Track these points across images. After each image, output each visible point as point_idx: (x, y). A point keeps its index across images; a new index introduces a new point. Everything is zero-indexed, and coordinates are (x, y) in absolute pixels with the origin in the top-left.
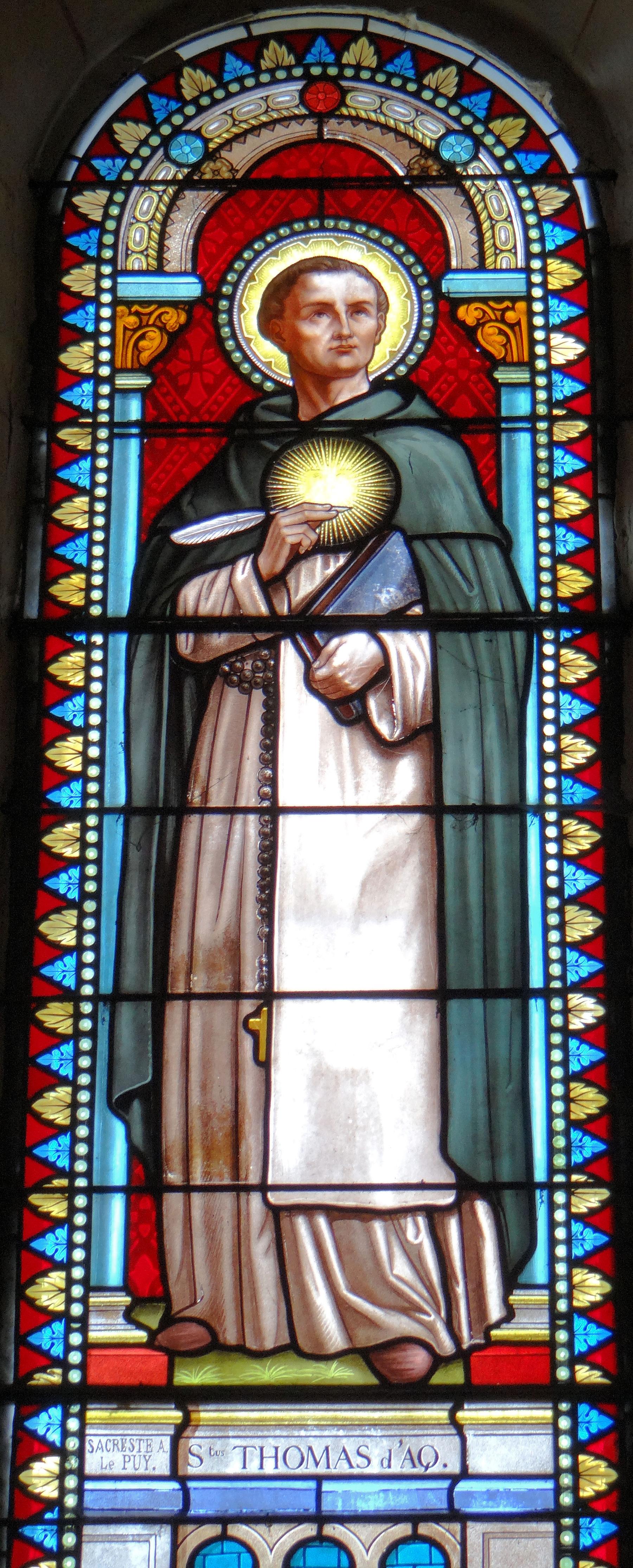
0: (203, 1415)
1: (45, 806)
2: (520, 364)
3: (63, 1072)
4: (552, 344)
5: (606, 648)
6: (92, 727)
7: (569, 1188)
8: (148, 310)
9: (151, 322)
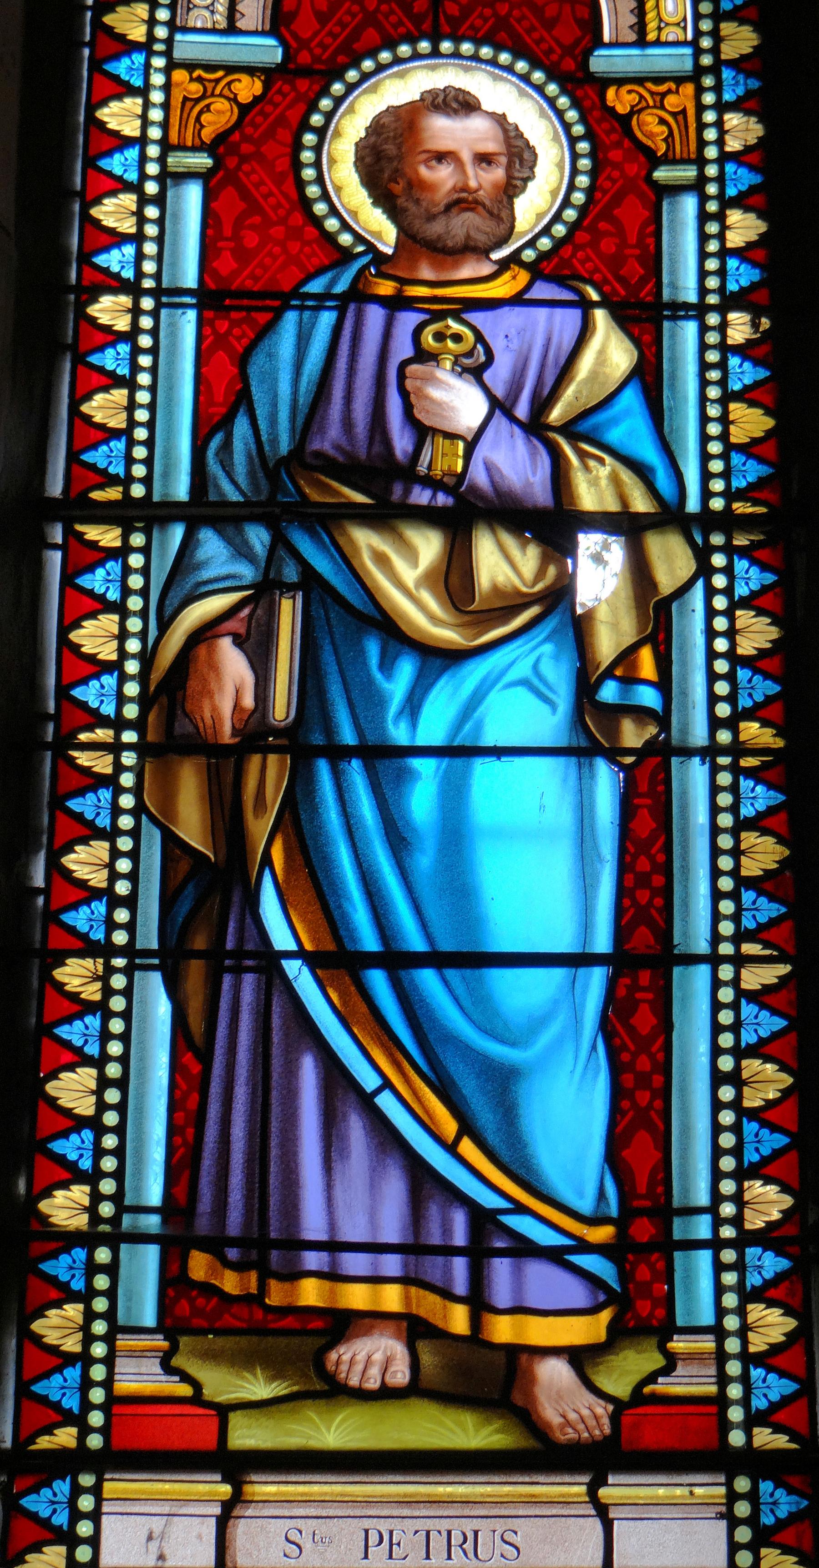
0: (258, 1488)
1: (35, 1226)
2: (685, 161)
3: (112, 424)
4: (728, 223)
5: (811, 1221)
6: (111, 1059)
7: (739, 961)
8: (212, 76)
9: (217, 92)
